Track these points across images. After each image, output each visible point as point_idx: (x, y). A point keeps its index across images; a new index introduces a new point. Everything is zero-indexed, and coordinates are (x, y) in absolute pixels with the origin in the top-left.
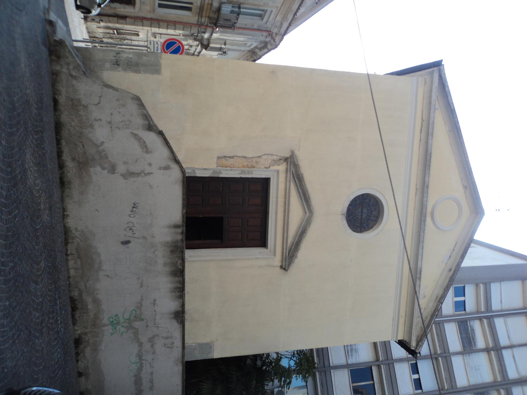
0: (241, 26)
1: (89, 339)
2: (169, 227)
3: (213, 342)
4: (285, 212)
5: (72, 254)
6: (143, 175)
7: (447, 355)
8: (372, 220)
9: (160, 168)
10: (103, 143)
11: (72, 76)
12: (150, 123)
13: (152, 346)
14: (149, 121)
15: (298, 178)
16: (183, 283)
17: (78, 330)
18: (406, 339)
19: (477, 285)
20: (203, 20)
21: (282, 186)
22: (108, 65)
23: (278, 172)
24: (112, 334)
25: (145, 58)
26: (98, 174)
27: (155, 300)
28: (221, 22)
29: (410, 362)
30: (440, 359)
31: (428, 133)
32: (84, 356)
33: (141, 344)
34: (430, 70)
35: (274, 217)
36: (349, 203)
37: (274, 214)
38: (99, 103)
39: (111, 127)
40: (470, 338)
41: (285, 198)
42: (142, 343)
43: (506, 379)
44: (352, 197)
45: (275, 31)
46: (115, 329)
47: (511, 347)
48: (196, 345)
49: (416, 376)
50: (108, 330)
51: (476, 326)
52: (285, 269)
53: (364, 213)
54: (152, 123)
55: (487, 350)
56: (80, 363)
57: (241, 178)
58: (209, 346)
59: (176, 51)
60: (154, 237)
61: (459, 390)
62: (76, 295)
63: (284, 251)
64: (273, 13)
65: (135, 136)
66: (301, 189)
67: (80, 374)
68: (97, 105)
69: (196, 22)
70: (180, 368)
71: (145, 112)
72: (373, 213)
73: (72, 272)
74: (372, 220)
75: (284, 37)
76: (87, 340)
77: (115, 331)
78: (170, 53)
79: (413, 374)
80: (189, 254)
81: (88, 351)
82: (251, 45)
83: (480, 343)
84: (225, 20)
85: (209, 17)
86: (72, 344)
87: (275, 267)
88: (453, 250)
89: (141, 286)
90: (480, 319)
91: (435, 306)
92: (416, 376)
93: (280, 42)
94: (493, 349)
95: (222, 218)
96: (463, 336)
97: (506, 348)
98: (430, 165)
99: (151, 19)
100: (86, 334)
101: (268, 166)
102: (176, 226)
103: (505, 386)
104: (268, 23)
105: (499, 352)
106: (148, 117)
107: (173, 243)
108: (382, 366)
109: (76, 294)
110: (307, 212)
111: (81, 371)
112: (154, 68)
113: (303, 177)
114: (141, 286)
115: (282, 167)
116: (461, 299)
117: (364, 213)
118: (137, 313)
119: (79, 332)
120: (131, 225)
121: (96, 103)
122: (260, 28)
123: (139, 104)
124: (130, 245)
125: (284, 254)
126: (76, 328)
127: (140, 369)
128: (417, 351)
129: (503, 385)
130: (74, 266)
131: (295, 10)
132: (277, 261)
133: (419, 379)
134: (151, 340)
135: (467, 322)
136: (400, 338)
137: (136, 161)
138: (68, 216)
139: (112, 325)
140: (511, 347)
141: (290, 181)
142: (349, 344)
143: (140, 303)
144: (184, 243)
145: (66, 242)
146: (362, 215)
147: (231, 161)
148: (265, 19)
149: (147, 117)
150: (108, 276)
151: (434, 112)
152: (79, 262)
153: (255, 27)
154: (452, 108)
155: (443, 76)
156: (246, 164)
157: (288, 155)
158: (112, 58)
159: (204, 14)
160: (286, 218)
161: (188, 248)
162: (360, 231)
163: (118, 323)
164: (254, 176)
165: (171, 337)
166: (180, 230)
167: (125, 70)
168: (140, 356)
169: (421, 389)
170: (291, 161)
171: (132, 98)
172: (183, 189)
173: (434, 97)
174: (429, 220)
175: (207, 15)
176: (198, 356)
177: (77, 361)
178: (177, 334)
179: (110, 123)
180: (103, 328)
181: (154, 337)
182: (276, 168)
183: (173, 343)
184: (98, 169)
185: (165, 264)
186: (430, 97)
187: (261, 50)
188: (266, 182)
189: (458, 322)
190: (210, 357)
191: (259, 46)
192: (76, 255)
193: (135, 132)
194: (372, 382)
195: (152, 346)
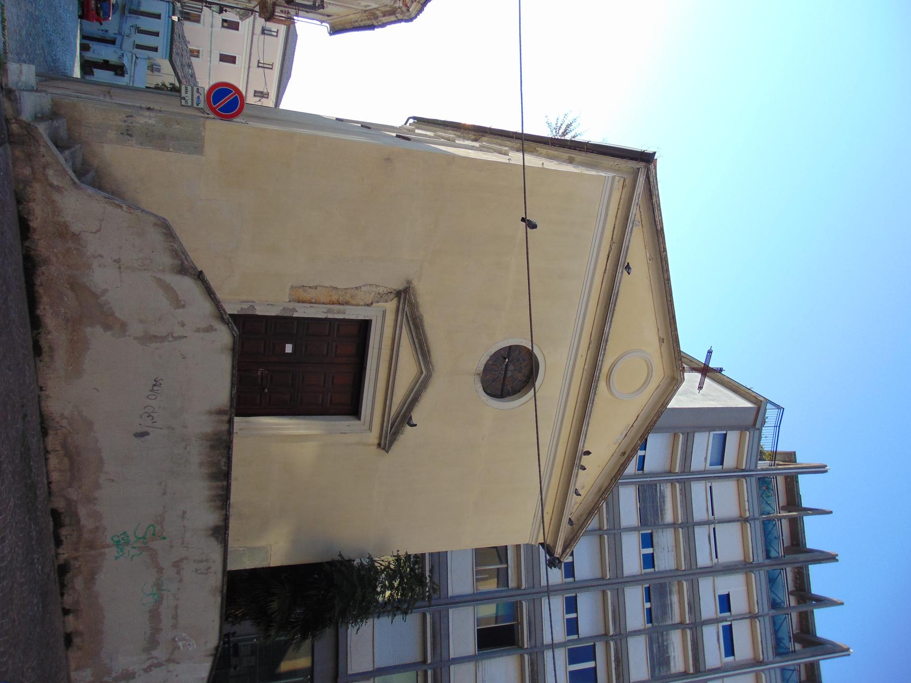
2: (210, 413)
6: (170, 339)
9: (198, 330)
10: (105, 291)
11: (51, 185)
12: (183, 263)
13: (178, 573)
15: (416, 325)
16: (228, 489)
19: (675, 436)
22: (112, 134)
23: (384, 312)
24: (117, 558)
25: (177, 126)
26: (98, 337)
27: (184, 512)
30: (606, 537)
31: (618, 264)
32: (73, 588)
33: (160, 570)
38: (99, 231)
39: (120, 268)
42: (163, 569)
43: (694, 567)
44: (494, 350)
50: (111, 553)
52: (384, 449)
53: (511, 373)
56: (65, 597)
57: (326, 319)
60: (186, 427)
65: (161, 283)
66: (418, 337)
67: (66, 612)
70: (219, 599)
71: (176, 246)
73: (55, 476)
76: (77, 566)
81: (79, 583)
87: (369, 445)
89: (164, 494)
90: (672, 482)
91: (595, 501)
94: (682, 526)
100: (76, 558)
107: (215, 434)
109: (59, 504)
111: (67, 607)
112: (195, 145)
113: (421, 321)
114: (164, 494)
116: (573, 615)
117: (511, 373)
119: (66, 555)
120: (150, 410)
123: (165, 234)
124: (146, 437)
126: (60, 551)
127: (159, 601)
129: (689, 575)
132: (373, 437)
133: (573, 562)
134: (177, 565)
135: (656, 485)
137: (160, 319)
138: (48, 396)
139: (117, 546)
145: (44, 432)
146: (505, 373)
150: (113, 481)
152: (66, 460)
157: (399, 286)
163: (127, 543)
164: (347, 317)
165: (207, 561)
168: (158, 585)
169: (574, 576)
170: (404, 296)
173: (634, 210)
174: (602, 384)
177: (62, 595)
178: (217, 556)
179: (117, 261)
181: (181, 560)
183: (209, 568)
184: (99, 330)
185: (201, 464)
187: (384, 16)
188: (364, 326)
193: (159, 276)
194: (505, 566)
195: (178, 573)
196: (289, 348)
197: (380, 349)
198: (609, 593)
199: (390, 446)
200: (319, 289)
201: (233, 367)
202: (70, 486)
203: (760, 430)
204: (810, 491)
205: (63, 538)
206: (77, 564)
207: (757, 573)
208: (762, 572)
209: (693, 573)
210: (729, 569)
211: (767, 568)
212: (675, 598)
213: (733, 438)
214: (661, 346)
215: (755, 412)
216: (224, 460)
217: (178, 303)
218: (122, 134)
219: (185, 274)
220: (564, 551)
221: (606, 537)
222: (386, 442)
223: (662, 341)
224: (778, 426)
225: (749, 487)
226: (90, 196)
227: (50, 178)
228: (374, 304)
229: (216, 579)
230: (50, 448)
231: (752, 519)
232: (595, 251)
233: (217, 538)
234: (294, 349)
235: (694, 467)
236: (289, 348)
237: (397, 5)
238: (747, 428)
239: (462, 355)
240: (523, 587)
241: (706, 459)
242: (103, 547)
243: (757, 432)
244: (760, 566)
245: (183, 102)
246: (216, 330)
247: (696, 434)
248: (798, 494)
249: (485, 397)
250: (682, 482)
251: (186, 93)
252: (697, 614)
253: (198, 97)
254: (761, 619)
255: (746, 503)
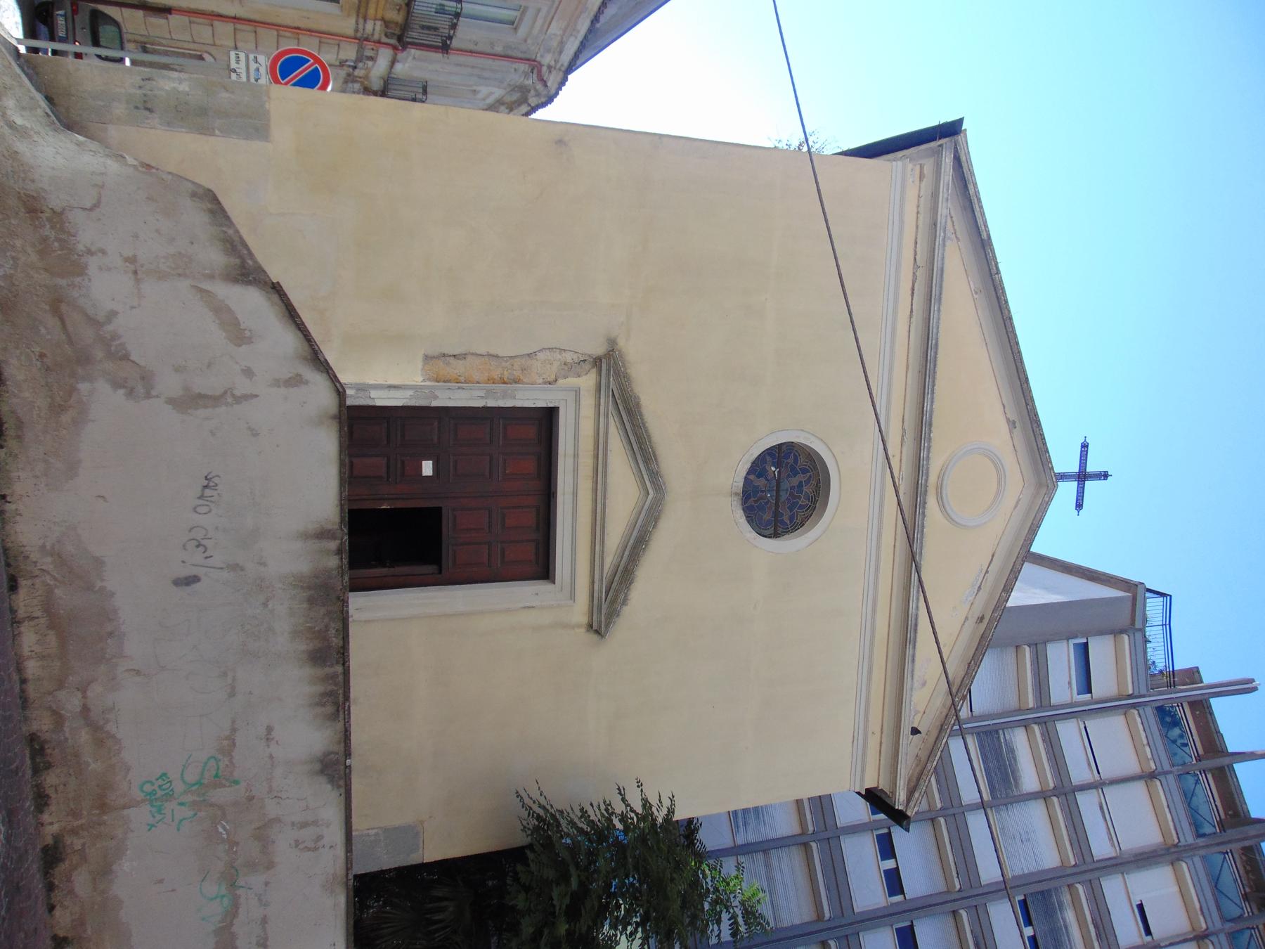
0: (463, 46)
1: (84, 845)
2: (305, 536)
3: (422, 822)
4: (595, 490)
5: (31, 618)
6: (230, 400)
7: (954, 812)
8: (801, 507)
9: (277, 383)
10: (113, 314)
11: (11, 125)
14: (241, 257)
15: (625, 407)
17: (52, 824)
18: (884, 785)
20: (369, 26)
21: (587, 427)
22: (119, 109)
23: (577, 392)
25: (225, 95)
26: (103, 400)
27: (270, 729)
28: (414, 34)
29: (876, 833)
30: (942, 820)
32: (71, 892)
34: (933, 144)
35: (569, 506)
36: (749, 465)
37: (569, 498)
38: (96, 206)
39: (135, 272)
40: (1006, 769)
41: (596, 457)
43: (1088, 859)
45: (547, 59)
46: (159, 812)
47: (1098, 785)
48: (377, 834)
49: (890, 864)
50: (139, 816)
51: (1019, 740)
52: (598, 632)
53: (784, 490)
54: (250, 262)
55: (1043, 795)
56: (58, 912)
58: (411, 833)
59: (310, 81)
61: (986, 890)
62: (45, 728)
63: (596, 587)
64: (542, 14)
68: (91, 210)
69: (350, 32)
70: (342, 899)
71: (231, 232)
72: (805, 489)
73: (32, 668)
74: (801, 507)
75: (570, 77)
77: (158, 817)
78: (294, 85)
79: (883, 859)
80: (359, 603)
81: (81, 881)
82: (492, 93)
83: (1029, 780)
84: (423, 27)
85: (383, 19)
86: (33, 865)
87: (573, 627)
88: (987, 572)
90: (1026, 725)
92: (890, 864)
93: (560, 89)
95: (440, 509)
96: (991, 765)
97: (1084, 788)
98: (935, 372)
99: (235, 18)
100: (74, 832)
101: (553, 377)
102: (322, 534)
103: (1088, 876)
104: (529, 41)
105: (1070, 797)
106: (240, 247)
107: (317, 577)
108: (814, 845)
109: (41, 723)
110: (651, 491)
111: (61, 934)
112: (253, 124)
113: (638, 405)
114: (232, 694)
115: (587, 381)
117: (784, 490)
118: (222, 765)
119: (55, 828)
121: (88, 205)
122: (510, 53)
123: (211, 211)
124: (196, 586)
125: (596, 595)
126: (46, 817)
128: (909, 813)
130: (37, 649)
131: (595, 9)
132: (579, 612)
133: (897, 869)
135: (997, 732)
136: (870, 783)
137: (209, 366)
140: (1098, 785)
141: (607, 416)
142: (751, 805)
143: (227, 738)
144: (346, 578)
147: (458, 368)
148: (522, 31)
149: (234, 245)
150: (138, 672)
151: (944, 245)
152: (52, 638)
153: (498, 49)
154: (984, 236)
155: (963, 159)
156: (496, 374)
157: (599, 349)
158: (133, 91)
159: (371, 11)
160: (599, 505)
161: (355, 587)
162: (775, 535)
163: (169, 796)
164: (519, 404)
165: (315, 823)
166: (333, 545)
167: (169, 124)
169: (902, 892)
170: (609, 365)
171: (194, 195)
172: (341, 436)
173: (943, 210)
174: (931, 501)
175: (379, 16)
176: (385, 860)
177: (51, 908)
178: (331, 813)
179: (132, 260)
180: (126, 812)
182: (572, 381)
183: (320, 838)
184: (103, 387)
186: (934, 209)
188: (548, 417)
189: (978, 734)
190: (414, 859)
191: (508, 99)
192: (42, 621)
193: (206, 286)
196: (427, 468)
197: (576, 456)
198: (963, 913)
199: (607, 626)
200: (469, 357)
201: (341, 452)
202: (61, 685)
203: (1142, 630)
204: (1235, 723)
205: (50, 792)
206: (77, 844)
207: (1190, 863)
208: (1197, 860)
209: (1088, 870)
210: (1144, 859)
211: (1202, 852)
212: (1070, 916)
213: (1101, 651)
214: (1011, 432)
215: (1130, 604)
216: (335, 625)
217: (239, 335)
218: (137, 108)
219: (249, 283)
220: (909, 800)
221: (942, 820)
222: (600, 623)
223: (1012, 424)
224: (1167, 624)
225: (1143, 722)
226: (79, 144)
227: (9, 112)
228: (561, 381)
229: (331, 861)
230: (21, 613)
231: (1160, 774)
232: (892, 283)
233: (332, 780)
234: (436, 468)
235: (1055, 700)
236: (427, 468)
237: (530, 82)
238: (1122, 631)
239: (708, 467)
240: (827, 915)
241: (1070, 683)
242: (125, 807)
243: (1139, 635)
244: (1191, 848)
245: (234, 76)
246: (307, 382)
247: (1048, 646)
248: (1218, 732)
249: (750, 534)
250: (1041, 722)
251: (238, 62)
252: (1111, 938)
253: (258, 70)
254: (1214, 938)
255: (1147, 749)
